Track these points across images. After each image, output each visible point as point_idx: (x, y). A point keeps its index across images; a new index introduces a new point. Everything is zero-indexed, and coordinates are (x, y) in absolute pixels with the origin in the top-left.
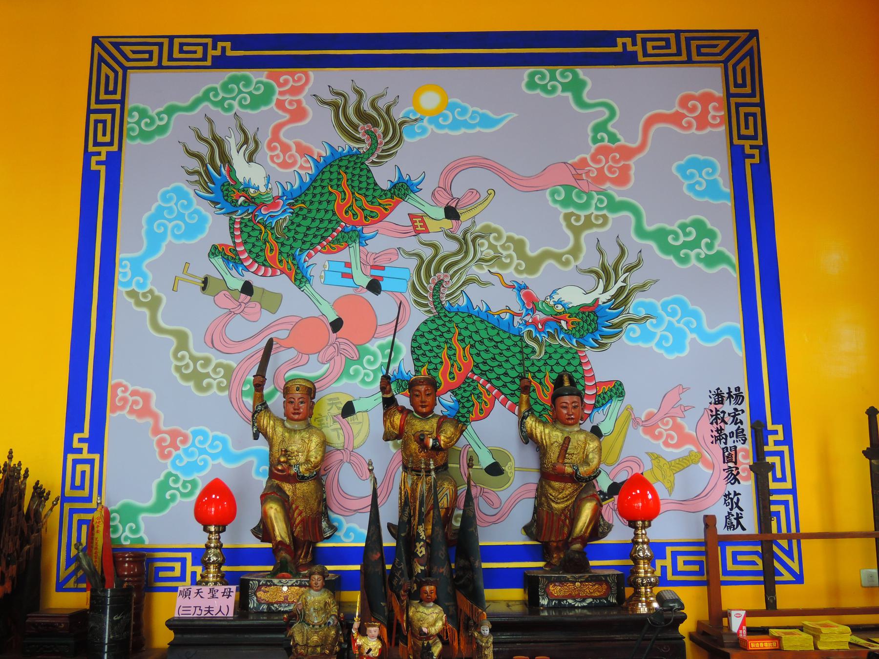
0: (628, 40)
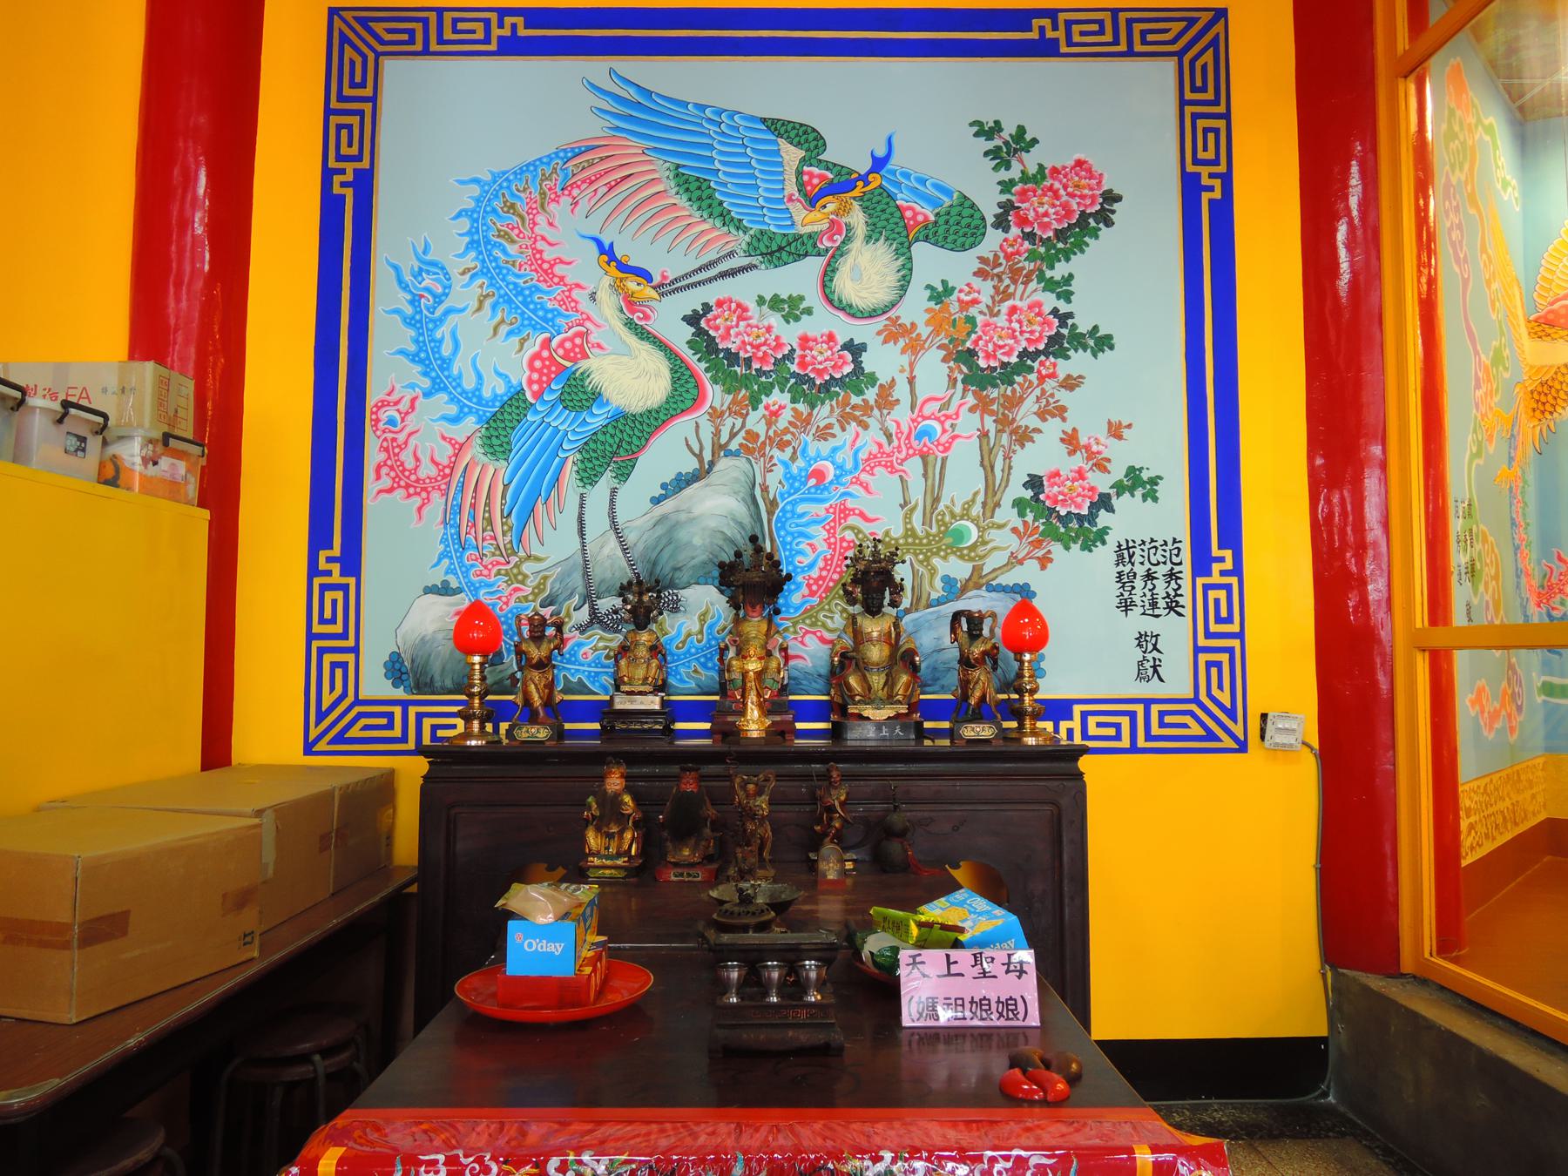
0: (1046, 22)
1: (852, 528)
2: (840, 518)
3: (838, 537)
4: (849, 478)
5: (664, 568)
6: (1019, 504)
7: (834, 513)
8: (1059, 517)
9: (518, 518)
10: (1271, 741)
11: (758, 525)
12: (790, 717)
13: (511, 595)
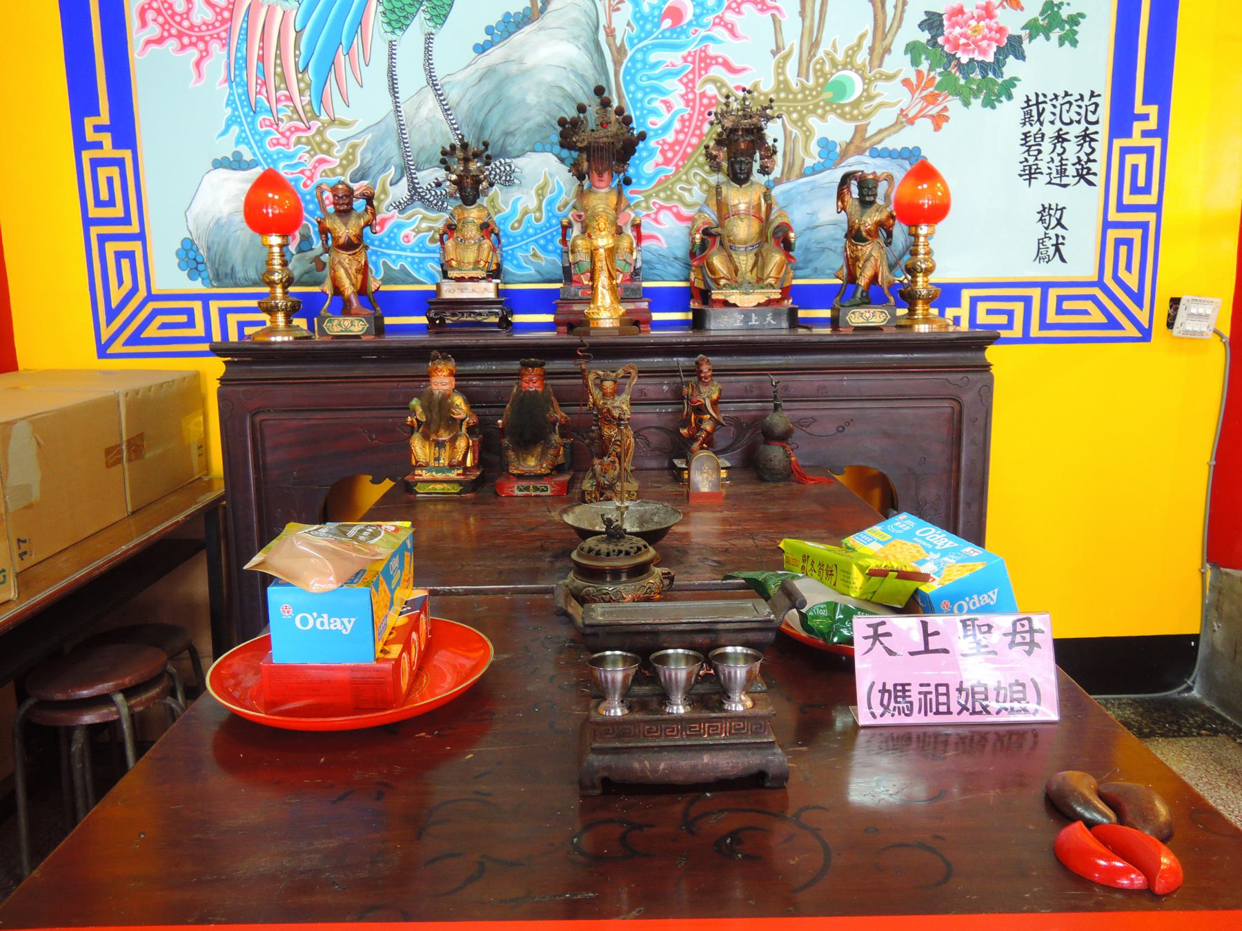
0: (1152, 124)
1: (714, 81)
2: (700, 69)
3: (698, 92)
4: (711, 17)
5: (493, 134)
6: (913, 50)
7: (693, 62)
8: (960, 65)
9: (317, 72)
10: (1181, 329)
11: (603, 77)
12: (645, 305)
13: (315, 167)
